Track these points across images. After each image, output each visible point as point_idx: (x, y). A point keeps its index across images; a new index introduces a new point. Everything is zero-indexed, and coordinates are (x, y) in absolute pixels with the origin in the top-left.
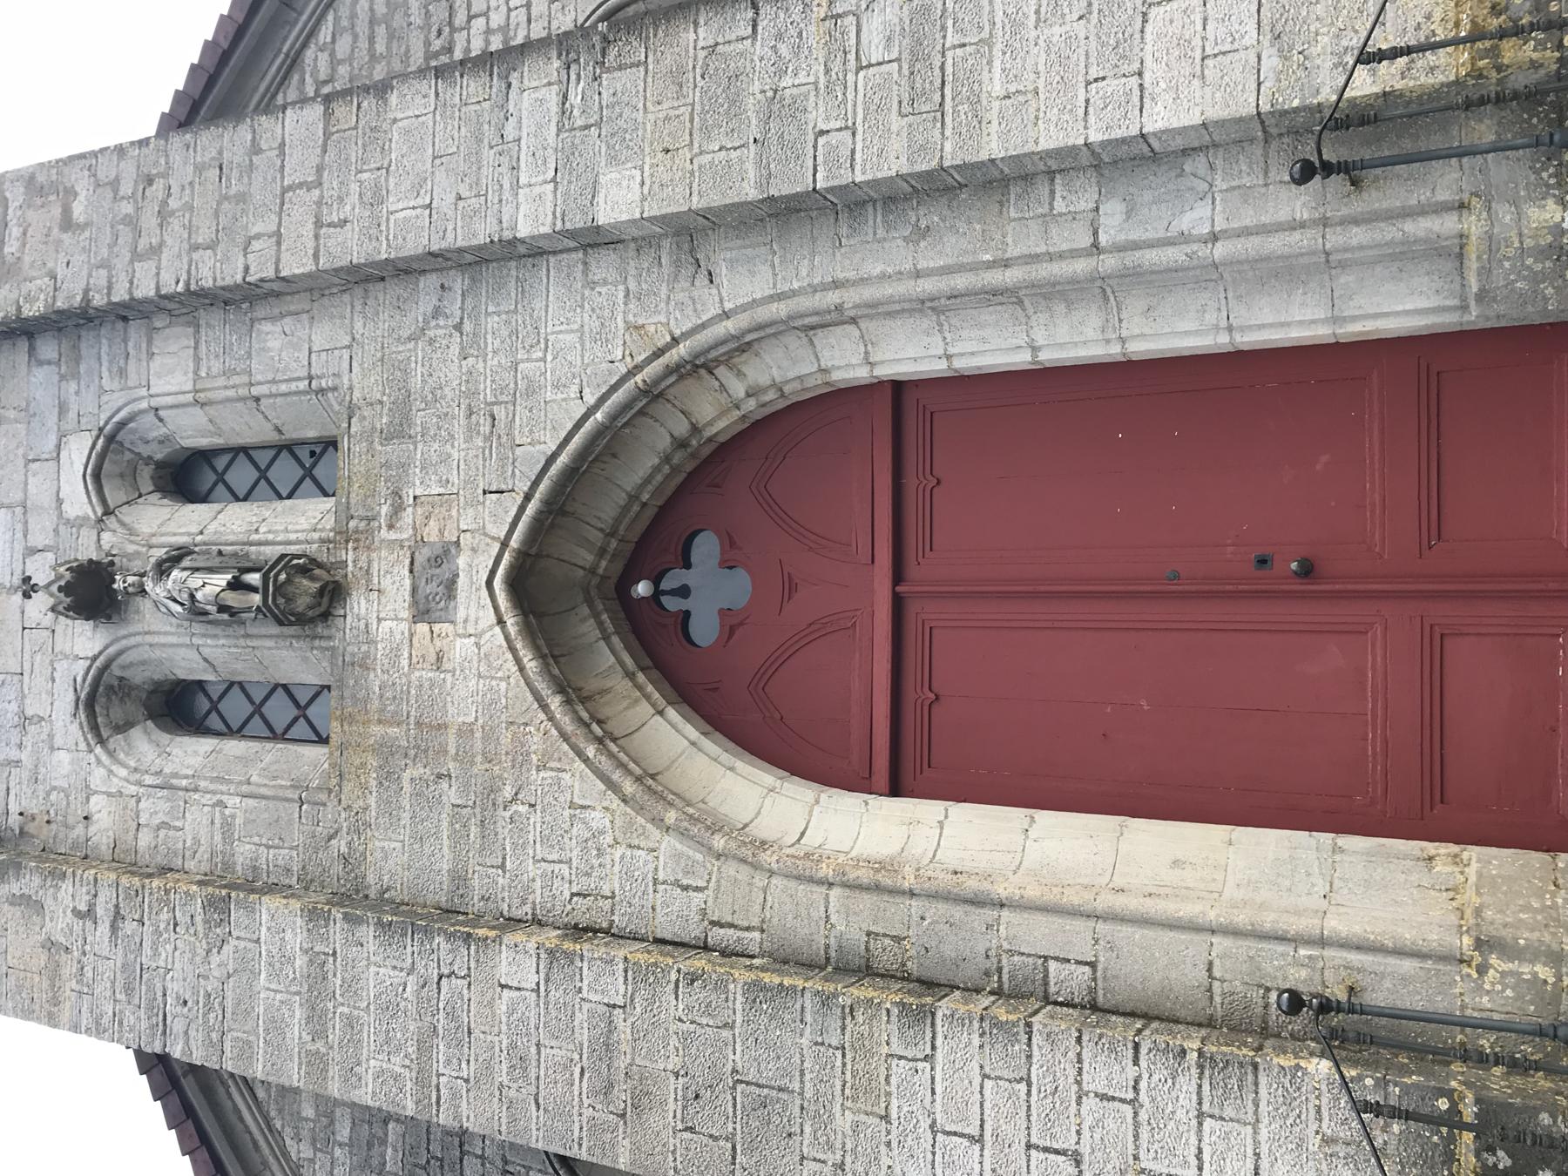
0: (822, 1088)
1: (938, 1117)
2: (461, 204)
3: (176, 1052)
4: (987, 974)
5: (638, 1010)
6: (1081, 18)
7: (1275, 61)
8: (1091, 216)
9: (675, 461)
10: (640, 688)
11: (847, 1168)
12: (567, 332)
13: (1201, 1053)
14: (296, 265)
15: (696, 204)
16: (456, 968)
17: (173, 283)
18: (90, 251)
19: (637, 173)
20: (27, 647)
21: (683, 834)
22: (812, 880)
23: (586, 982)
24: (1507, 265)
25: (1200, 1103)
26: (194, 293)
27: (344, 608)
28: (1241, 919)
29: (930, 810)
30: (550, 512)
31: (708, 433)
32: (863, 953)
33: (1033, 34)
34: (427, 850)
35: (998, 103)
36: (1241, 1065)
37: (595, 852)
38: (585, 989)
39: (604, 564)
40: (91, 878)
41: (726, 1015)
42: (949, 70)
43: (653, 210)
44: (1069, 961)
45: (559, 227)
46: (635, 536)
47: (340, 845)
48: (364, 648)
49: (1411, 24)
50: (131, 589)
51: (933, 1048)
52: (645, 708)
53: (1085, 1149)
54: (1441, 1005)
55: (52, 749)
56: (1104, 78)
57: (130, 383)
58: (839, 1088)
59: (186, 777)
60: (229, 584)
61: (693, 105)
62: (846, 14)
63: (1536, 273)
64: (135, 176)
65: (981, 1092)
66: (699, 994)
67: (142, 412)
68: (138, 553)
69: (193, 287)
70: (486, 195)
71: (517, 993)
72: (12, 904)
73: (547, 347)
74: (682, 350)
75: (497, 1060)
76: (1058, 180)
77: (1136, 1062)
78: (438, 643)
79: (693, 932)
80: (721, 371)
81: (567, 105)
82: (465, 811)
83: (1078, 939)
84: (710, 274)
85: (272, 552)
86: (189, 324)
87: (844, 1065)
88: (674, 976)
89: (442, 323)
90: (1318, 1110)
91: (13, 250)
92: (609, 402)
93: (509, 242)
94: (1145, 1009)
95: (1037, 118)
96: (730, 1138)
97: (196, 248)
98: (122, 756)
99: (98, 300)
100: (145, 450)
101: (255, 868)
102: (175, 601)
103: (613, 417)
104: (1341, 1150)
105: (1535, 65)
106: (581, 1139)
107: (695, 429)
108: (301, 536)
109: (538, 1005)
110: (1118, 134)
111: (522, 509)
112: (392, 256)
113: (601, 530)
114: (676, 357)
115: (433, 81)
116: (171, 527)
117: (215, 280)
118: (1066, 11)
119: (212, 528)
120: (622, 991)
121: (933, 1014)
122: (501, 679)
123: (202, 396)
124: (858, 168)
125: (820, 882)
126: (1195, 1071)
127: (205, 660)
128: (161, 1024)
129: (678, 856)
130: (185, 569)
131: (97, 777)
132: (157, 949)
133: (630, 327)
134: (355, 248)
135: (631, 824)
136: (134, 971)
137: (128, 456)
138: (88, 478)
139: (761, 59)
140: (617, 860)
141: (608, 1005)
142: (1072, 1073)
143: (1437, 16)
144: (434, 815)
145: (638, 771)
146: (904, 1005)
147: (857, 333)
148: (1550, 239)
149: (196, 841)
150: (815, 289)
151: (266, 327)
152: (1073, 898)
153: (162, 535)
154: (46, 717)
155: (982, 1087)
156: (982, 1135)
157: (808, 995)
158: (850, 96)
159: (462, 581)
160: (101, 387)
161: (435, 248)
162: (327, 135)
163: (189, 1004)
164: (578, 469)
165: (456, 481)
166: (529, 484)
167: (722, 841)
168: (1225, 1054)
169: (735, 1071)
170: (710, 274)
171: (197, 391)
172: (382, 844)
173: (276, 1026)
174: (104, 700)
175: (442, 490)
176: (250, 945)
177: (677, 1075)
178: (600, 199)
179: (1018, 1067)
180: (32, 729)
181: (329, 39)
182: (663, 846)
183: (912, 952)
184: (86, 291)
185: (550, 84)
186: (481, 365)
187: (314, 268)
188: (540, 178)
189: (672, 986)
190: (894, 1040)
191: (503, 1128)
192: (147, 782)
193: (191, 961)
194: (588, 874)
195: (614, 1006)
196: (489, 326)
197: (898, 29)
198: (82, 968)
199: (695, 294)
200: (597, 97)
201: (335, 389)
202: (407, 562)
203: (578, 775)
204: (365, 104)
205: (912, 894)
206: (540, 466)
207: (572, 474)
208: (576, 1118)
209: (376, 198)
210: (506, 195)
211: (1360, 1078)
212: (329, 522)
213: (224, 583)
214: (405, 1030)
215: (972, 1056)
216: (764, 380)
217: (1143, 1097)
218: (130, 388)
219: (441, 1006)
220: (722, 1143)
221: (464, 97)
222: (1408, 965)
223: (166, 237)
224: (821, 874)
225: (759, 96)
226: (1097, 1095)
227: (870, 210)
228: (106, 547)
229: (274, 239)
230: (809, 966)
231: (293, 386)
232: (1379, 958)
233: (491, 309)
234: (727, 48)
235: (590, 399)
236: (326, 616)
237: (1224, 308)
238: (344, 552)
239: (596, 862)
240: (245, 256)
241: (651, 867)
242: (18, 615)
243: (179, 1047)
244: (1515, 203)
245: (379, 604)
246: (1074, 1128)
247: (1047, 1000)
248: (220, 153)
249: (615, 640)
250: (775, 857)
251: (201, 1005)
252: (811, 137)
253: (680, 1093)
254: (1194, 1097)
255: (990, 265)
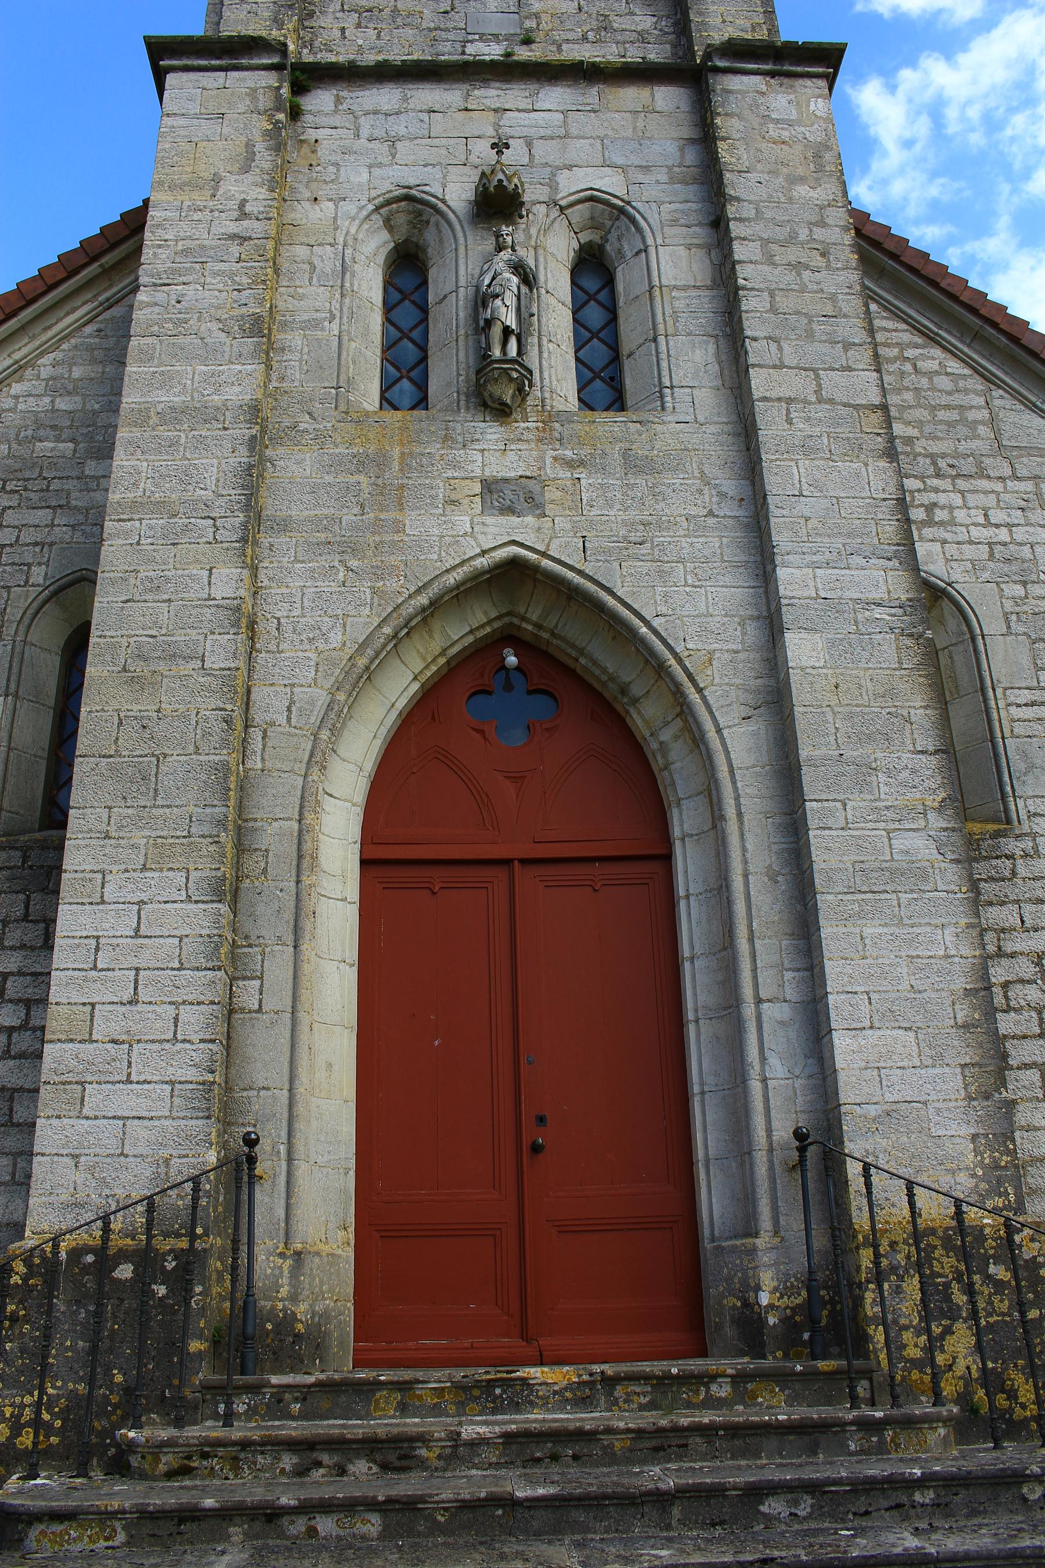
0: (160, 822)
1: (150, 906)
2: (802, 521)
3: (142, 296)
4: (247, 937)
5: (202, 680)
6: (912, 986)
7: (873, 1113)
8: (781, 997)
9: (610, 684)
10: (434, 660)
11: (106, 841)
12: (707, 603)
13: (213, 1083)
14: (759, 382)
15: (798, 710)
16: (222, 531)
17: (745, 276)
18: (770, 202)
19: (822, 664)
20: (452, 141)
21: (329, 707)
22: (302, 807)
23: (219, 637)
24: (738, 1262)
25: (180, 1083)
26: (736, 294)
27: (491, 421)
28: (300, 1109)
29: (353, 891)
30: (569, 589)
31: (632, 710)
32: (253, 847)
33: (904, 954)
34: (306, 498)
35: (858, 931)
36: (208, 1109)
37: (311, 636)
38: (215, 637)
39: (530, 628)
40: (271, 215)
41: (204, 748)
42: (883, 896)
43: (795, 677)
44: (261, 994)
45: (784, 601)
46: (551, 650)
47: (305, 423)
48: (460, 439)
49: (889, 1195)
50: (501, 239)
51: (196, 902)
52: (418, 665)
53: (140, 1007)
54: (258, 1231)
55: (370, 167)
56: (870, 1003)
57: (666, 229)
58: (162, 834)
59: (352, 285)
60: (508, 327)
61: (869, 706)
62: (927, 821)
63: (732, 1279)
64: (828, 241)
65: (169, 936)
66: (217, 727)
67: (644, 239)
68: (530, 237)
69: (741, 292)
70: (809, 541)
71: (206, 583)
72: (247, 145)
73: (695, 587)
74: (694, 696)
75: (155, 568)
76: (806, 973)
77: (202, 1041)
78: (466, 501)
79: (258, 716)
80: (679, 723)
81: (873, 607)
82: (337, 527)
83: (278, 999)
84: (749, 718)
85: (532, 360)
86: (714, 281)
87: (178, 837)
88: (229, 707)
89: (714, 499)
90: (185, 1156)
91: (771, 133)
92: (654, 638)
93: (773, 561)
94: (233, 1046)
95: (847, 959)
96: (118, 754)
97: (772, 295)
98: (366, 226)
99: (731, 210)
100: (613, 236)
101: (283, 349)
102: (493, 278)
103: (642, 641)
104: (162, 1170)
105: (858, 1268)
106: (105, 637)
107: (635, 701)
108: (546, 382)
109: (199, 599)
110: (833, 1014)
111: (571, 568)
112: (764, 464)
113: (556, 626)
114: (688, 692)
115: (894, 497)
116: (552, 264)
117: (747, 312)
118: (917, 976)
119: (552, 300)
120: (215, 666)
121: (220, 901)
122: (439, 555)
123: (657, 292)
124: (819, 832)
125: (301, 814)
126: (201, 1079)
127: (445, 297)
128: (161, 281)
129: (312, 702)
130: (519, 288)
131: (348, 208)
132: (219, 275)
133: (711, 653)
134: (771, 432)
135: (334, 664)
136: (201, 257)
137: (608, 223)
138: (589, 192)
139: (899, 758)
140: (307, 654)
141: (203, 656)
142: (190, 998)
143: (893, 1210)
144: (333, 503)
145: (373, 667)
146: (224, 880)
147: (706, 828)
148: (752, 1285)
149: (302, 297)
150: (737, 798)
151: (711, 348)
152: (304, 994)
153: (545, 258)
154: (395, 160)
155: (173, 936)
156: (140, 937)
157: (224, 810)
158: (870, 825)
159: (514, 520)
160: (663, 203)
161: (770, 499)
162: (857, 407)
163: (178, 306)
164: (603, 612)
165: (592, 514)
166: (591, 574)
167: (325, 737)
168: (214, 1098)
169: (165, 756)
170: (749, 718)
171: (661, 287)
172: (308, 459)
173: (166, 381)
174: (411, 209)
175: (585, 501)
176: (227, 357)
177: (158, 711)
178: (804, 635)
179: (189, 961)
180: (385, 148)
181: (949, 370)
182: (318, 690)
183: (257, 883)
184: (738, 199)
185: (889, 592)
186: (682, 533)
187: (755, 397)
188: (820, 586)
189: (222, 706)
190: (199, 873)
191: (107, 575)
192: (347, 251)
193: (211, 305)
194: (295, 631)
195: (203, 661)
196: (712, 539)
197: (914, 859)
198: (200, 210)
199: (735, 706)
200: (878, 630)
201: (663, 409)
202: (528, 474)
203: (368, 620)
204: (880, 439)
205: (298, 882)
206: (604, 582)
207: (600, 607)
208: (119, 633)
209: (808, 449)
210: (808, 558)
211: (209, 1182)
212: (559, 405)
213: (508, 323)
214: (172, 490)
215: (194, 930)
216: (673, 756)
217: (179, 1046)
218: (662, 228)
219: (192, 520)
220: (113, 747)
221: (882, 522)
222: (281, 1212)
223: (780, 268)
224: (306, 814)
225: (872, 757)
226: (177, 1015)
227: (792, 839)
228: (535, 209)
229: (778, 363)
230: (240, 807)
231: (665, 372)
232: (283, 1195)
233: (725, 540)
234: (908, 732)
235: (656, 623)
236: (485, 405)
237: (718, 1088)
238: (535, 419)
239: (304, 637)
240: (765, 338)
241: (303, 681)
242: (477, 134)
243: (145, 299)
244: (776, 1264)
245: (495, 450)
246: (152, 999)
247: (233, 979)
248: (845, 316)
249: (471, 639)
250: (316, 778)
251: (179, 316)
252: (842, 797)
253: (145, 714)
254: (183, 1079)
255: (751, 932)
